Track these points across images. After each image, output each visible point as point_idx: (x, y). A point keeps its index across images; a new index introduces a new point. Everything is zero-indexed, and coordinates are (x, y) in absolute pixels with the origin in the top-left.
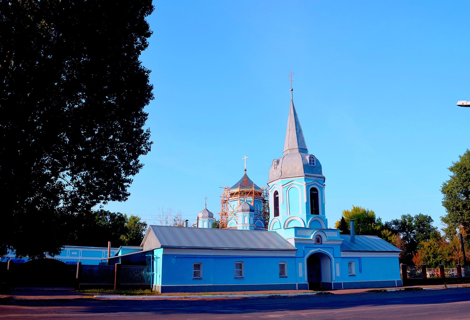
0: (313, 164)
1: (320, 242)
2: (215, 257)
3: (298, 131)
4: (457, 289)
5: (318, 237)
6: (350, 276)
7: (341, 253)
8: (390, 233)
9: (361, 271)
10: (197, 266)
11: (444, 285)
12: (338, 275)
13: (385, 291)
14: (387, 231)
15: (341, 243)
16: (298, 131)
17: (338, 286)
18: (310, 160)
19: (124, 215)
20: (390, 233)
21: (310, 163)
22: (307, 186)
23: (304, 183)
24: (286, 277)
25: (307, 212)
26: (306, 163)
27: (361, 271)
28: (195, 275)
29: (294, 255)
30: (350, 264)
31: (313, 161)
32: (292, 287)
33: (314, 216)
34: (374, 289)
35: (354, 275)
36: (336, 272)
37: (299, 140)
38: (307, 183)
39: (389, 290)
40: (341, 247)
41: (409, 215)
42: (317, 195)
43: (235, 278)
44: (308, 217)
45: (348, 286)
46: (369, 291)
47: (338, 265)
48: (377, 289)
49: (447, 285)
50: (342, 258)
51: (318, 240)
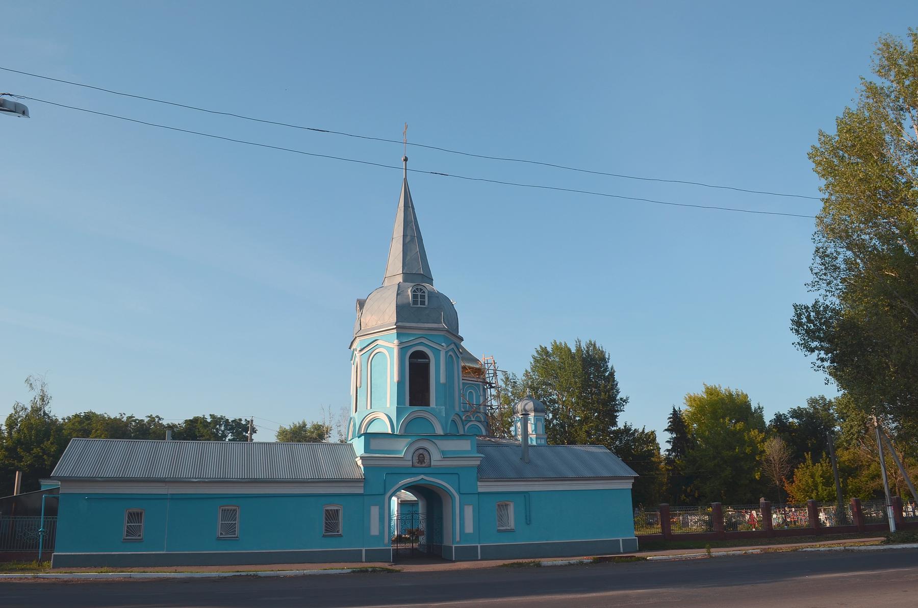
0: (423, 303)
1: (427, 461)
2: (174, 498)
3: (408, 239)
4: (746, 556)
5: (421, 451)
6: (499, 531)
7: (479, 483)
8: (762, 436)
9: (528, 521)
10: (135, 516)
11: (705, 550)
12: (469, 528)
13: (538, 565)
14: (756, 431)
15: (478, 463)
16: (408, 239)
17: (468, 554)
18: (415, 296)
19: (804, 405)
20: (762, 436)
21: (415, 302)
22: (402, 350)
23: (396, 342)
24: (341, 536)
25: (399, 402)
26: (405, 301)
27: (528, 521)
28: (129, 533)
29: (361, 491)
30: (503, 507)
31: (423, 297)
32: (354, 556)
33: (416, 408)
34: (515, 561)
35: (512, 531)
36: (463, 523)
37: (408, 258)
38: (401, 343)
39: (546, 562)
40: (478, 472)
41: (823, 398)
42: (426, 367)
43: (219, 539)
44: (399, 412)
45: (489, 553)
46: (504, 565)
47: (469, 511)
48: (520, 561)
49: (712, 550)
50: (479, 493)
51: (421, 457)
